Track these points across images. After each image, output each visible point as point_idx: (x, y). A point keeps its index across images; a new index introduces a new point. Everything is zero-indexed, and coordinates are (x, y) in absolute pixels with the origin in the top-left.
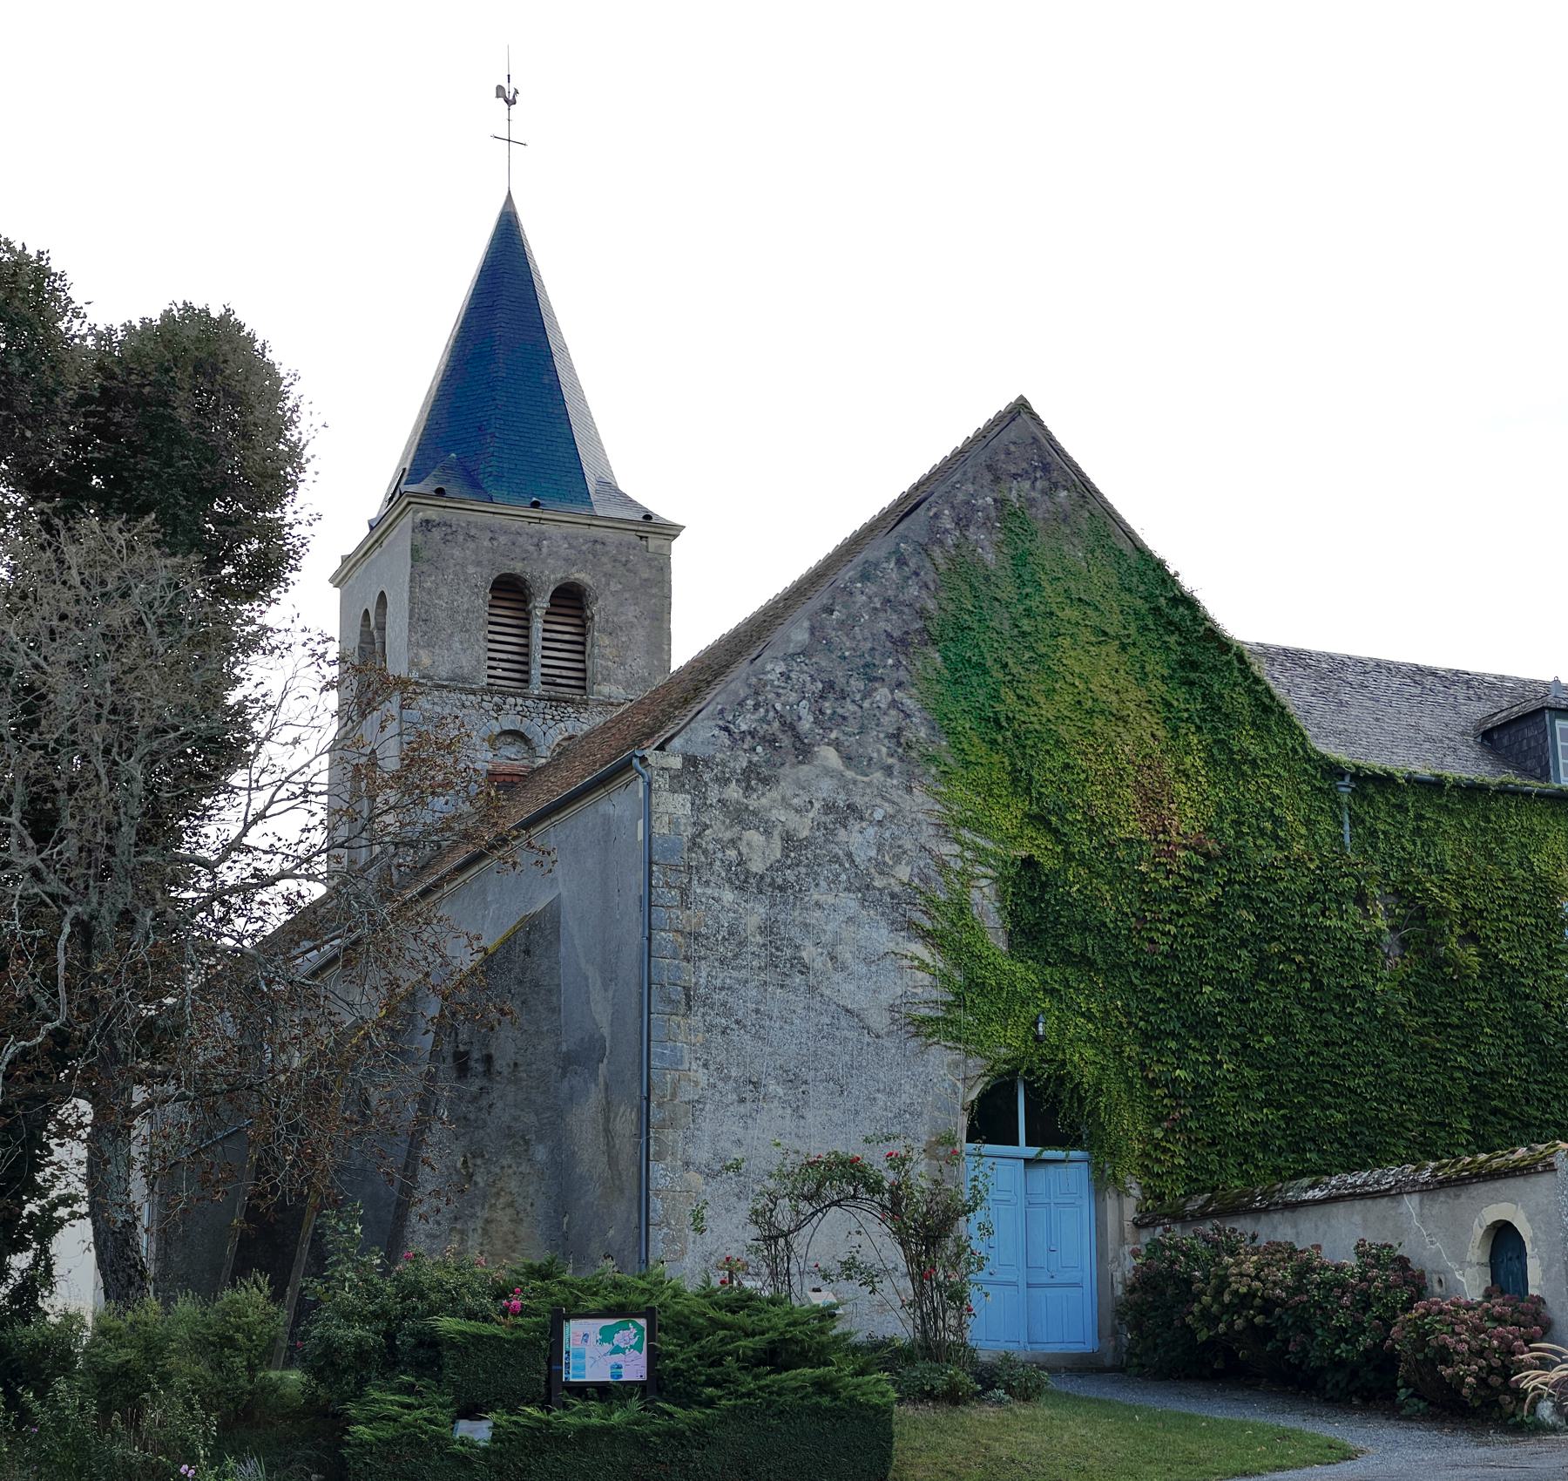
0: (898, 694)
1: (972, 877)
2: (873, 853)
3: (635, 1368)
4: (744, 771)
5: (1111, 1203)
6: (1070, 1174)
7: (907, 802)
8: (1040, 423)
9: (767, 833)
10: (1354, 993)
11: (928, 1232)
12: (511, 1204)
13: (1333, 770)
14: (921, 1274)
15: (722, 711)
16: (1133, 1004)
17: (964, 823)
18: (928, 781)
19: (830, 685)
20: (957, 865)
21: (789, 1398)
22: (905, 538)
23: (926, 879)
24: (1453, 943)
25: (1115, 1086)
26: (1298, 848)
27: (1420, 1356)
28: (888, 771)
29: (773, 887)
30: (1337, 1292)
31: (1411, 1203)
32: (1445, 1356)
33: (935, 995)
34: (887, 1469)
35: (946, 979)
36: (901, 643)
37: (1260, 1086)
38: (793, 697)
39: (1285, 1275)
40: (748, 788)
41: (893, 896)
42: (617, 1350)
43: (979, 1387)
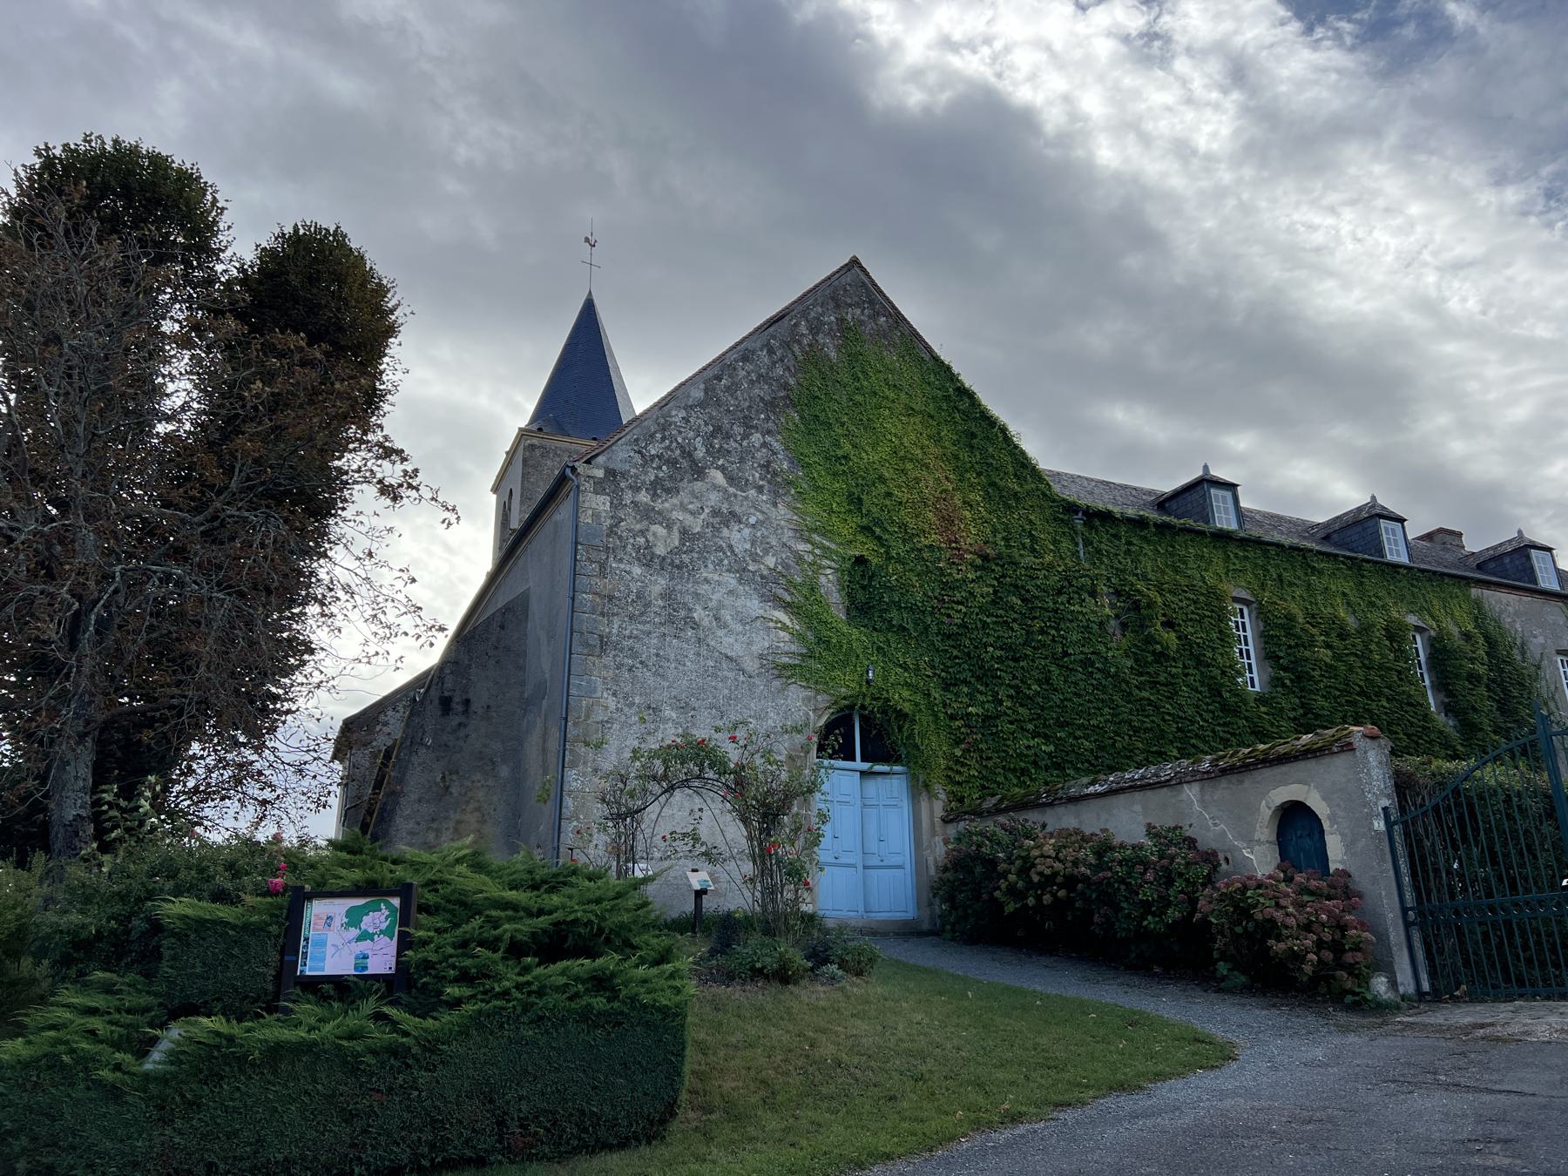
0: (768, 439)
1: (820, 567)
2: (748, 546)
3: (382, 960)
4: (651, 483)
5: (924, 805)
6: (892, 787)
7: (773, 513)
8: (867, 274)
9: (669, 527)
10: (1093, 657)
11: (769, 811)
12: (478, 809)
13: (1071, 508)
14: (762, 855)
15: (636, 440)
16: (937, 660)
17: (815, 530)
18: (788, 499)
19: (718, 429)
20: (809, 558)
21: (552, 999)
22: (774, 337)
23: (787, 567)
24: (1159, 626)
25: (924, 718)
26: (1048, 558)
27: (1239, 930)
28: (760, 489)
29: (672, 565)
30: (1139, 868)
31: (1191, 792)
32: (1270, 928)
33: (793, 648)
34: (676, 1091)
35: (801, 638)
36: (771, 405)
37: (1030, 721)
38: (691, 434)
39: (1086, 853)
40: (655, 496)
41: (762, 577)
42: (365, 936)
43: (810, 964)
